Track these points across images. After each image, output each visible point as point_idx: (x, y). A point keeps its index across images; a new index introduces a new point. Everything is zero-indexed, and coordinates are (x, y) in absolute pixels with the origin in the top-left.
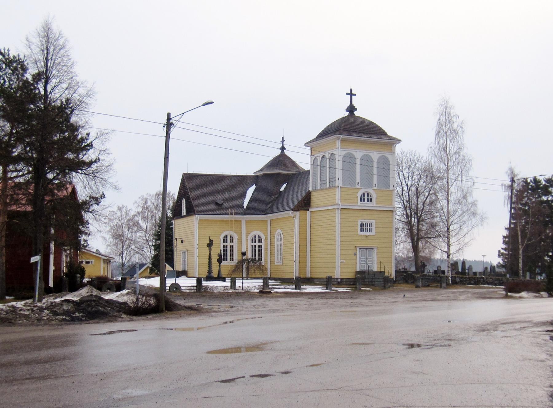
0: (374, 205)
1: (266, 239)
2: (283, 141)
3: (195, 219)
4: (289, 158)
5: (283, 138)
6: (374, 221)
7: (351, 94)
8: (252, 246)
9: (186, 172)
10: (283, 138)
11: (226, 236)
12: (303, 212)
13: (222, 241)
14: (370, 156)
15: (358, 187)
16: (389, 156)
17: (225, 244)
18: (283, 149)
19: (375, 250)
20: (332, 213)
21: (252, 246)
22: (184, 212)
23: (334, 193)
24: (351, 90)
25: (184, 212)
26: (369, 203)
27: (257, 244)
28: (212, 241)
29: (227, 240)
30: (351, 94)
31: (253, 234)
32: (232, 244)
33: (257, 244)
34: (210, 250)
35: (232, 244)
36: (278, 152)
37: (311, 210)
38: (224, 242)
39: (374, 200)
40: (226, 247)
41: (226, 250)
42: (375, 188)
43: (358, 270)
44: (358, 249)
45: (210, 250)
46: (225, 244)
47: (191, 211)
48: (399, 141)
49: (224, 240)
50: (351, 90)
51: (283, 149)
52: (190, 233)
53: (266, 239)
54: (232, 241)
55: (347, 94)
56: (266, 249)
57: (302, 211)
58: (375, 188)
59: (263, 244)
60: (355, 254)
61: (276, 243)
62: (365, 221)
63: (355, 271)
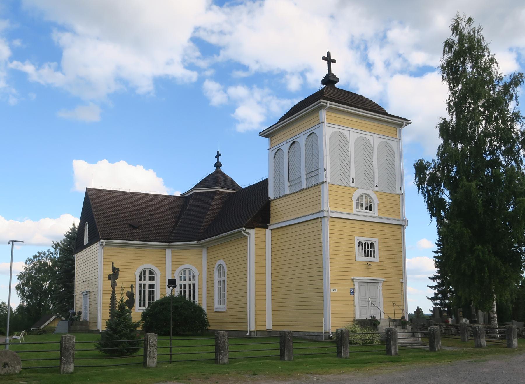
0: (377, 215)
1: (200, 276)
2: (218, 155)
3: (97, 246)
4: (227, 177)
5: (218, 152)
6: (377, 240)
7: (329, 60)
10: (218, 152)
11: (144, 272)
12: (260, 231)
13: (138, 278)
14: (368, 140)
15: (353, 185)
16: (394, 145)
17: (142, 282)
18: (218, 165)
19: (381, 284)
20: (316, 225)
22: (86, 241)
23: (317, 194)
24: (329, 54)
25: (86, 241)
26: (368, 211)
28: (118, 270)
32: (152, 282)
34: (114, 286)
35: (152, 282)
37: (271, 227)
38: (140, 280)
39: (375, 207)
40: (144, 287)
42: (377, 189)
43: (358, 317)
44: (356, 284)
45: (114, 286)
47: (93, 240)
48: (408, 122)
49: (141, 277)
50: (329, 54)
51: (218, 165)
55: (324, 58)
56: (200, 288)
57: (256, 229)
58: (377, 189)
59: (196, 282)
60: (353, 293)
61: (216, 279)
62: (364, 240)
63: (352, 319)
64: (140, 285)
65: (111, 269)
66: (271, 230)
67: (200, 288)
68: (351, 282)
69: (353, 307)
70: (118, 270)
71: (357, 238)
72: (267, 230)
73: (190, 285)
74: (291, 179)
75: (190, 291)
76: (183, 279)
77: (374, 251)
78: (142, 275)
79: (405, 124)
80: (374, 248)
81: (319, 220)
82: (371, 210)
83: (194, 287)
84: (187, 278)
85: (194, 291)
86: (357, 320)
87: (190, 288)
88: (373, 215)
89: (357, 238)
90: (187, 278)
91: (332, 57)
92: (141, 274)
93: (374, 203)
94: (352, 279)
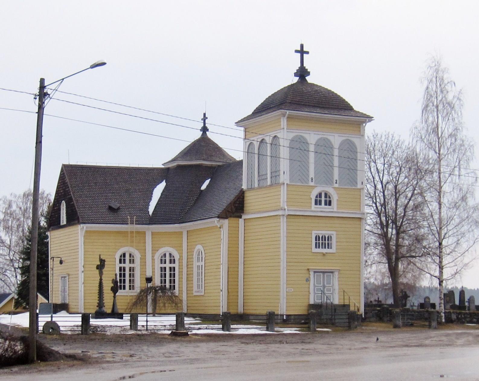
0: (335, 210)
1: (181, 259)
2: (205, 118)
3: (80, 230)
5: (205, 114)
6: (334, 233)
7: (302, 52)
10: (205, 114)
11: (124, 255)
12: (233, 220)
17: (122, 265)
18: (205, 129)
19: (336, 274)
24: (302, 46)
25: (64, 220)
26: (328, 207)
28: (104, 261)
29: (124, 260)
30: (302, 52)
31: (162, 251)
32: (132, 265)
34: (101, 274)
37: (244, 217)
38: (120, 262)
42: (336, 186)
43: (312, 302)
44: (312, 273)
45: (101, 274)
46: (122, 265)
48: (369, 118)
49: (120, 260)
50: (302, 46)
51: (205, 129)
52: (73, 249)
53: (181, 259)
54: (132, 261)
55: (297, 51)
56: (181, 272)
57: (230, 218)
58: (336, 186)
59: (176, 265)
63: (307, 304)
64: (120, 268)
65: (98, 260)
66: (244, 219)
67: (181, 272)
68: (307, 272)
69: (307, 293)
70: (104, 261)
71: (314, 232)
72: (240, 219)
73: (170, 268)
74: (260, 174)
75: (171, 274)
76: (163, 262)
77: (331, 243)
78: (122, 258)
79: (367, 120)
80: (331, 240)
81: (278, 217)
82: (330, 204)
83: (174, 271)
84: (168, 261)
85: (174, 274)
86: (310, 304)
87: (171, 271)
88: (332, 210)
89: (314, 232)
90: (168, 261)
91: (305, 49)
92: (121, 256)
93: (333, 200)
94: (308, 269)
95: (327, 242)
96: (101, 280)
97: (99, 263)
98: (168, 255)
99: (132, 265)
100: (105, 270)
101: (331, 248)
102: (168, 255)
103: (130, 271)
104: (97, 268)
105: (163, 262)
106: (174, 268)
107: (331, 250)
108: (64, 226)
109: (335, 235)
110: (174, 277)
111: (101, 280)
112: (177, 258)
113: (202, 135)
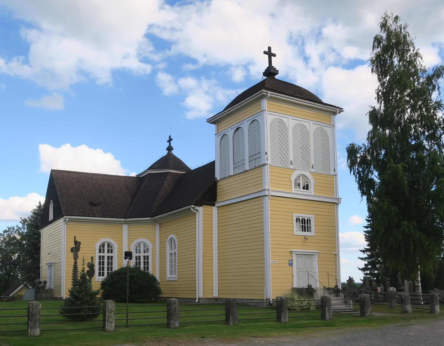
0: (313, 194)
2: (170, 140)
7: (270, 54)
8: (112, 252)
9: (55, 169)
10: (170, 137)
11: (103, 245)
13: (97, 251)
14: (305, 126)
15: (291, 167)
16: (328, 130)
17: (102, 254)
18: (170, 149)
19: (316, 256)
20: (259, 202)
21: (112, 252)
22: (51, 217)
24: (269, 48)
26: (305, 190)
27: (106, 254)
28: (80, 243)
30: (270, 54)
32: (110, 255)
33: (106, 254)
36: (165, 153)
37: (217, 205)
39: (311, 187)
41: (103, 262)
42: (313, 170)
43: (295, 286)
44: (294, 256)
49: (100, 250)
50: (269, 48)
51: (170, 149)
54: (110, 251)
56: (154, 260)
57: (204, 206)
58: (313, 170)
59: (150, 254)
60: (291, 265)
61: (168, 251)
66: (218, 207)
67: (154, 260)
68: (290, 254)
70: (80, 243)
71: (295, 215)
72: (214, 207)
73: (144, 257)
74: (236, 161)
75: (145, 262)
76: (138, 252)
77: (310, 227)
79: (338, 112)
80: (310, 224)
82: (307, 189)
84: (142, 251)
86: (295, 289)
89: (295, 215)
90: (142, 251)
92: (100, 247)
94: (291, 252)
95: (306, 225)
96: (76, 263)
97: (74, 246)
98: (142, 245)
99: (110, 255)
100: (80, 254)
101: (310, 231)
102: (142, 245)
103: (108, 259)
104: (72, 250)
105: (138, 252)
106: (148, 256)
107: (309, 233)
108: (52, 222)
109: (313, 218)
110: (148, 264)
111: (76, 263)
112: (150, 246)
113: (168, 152)
